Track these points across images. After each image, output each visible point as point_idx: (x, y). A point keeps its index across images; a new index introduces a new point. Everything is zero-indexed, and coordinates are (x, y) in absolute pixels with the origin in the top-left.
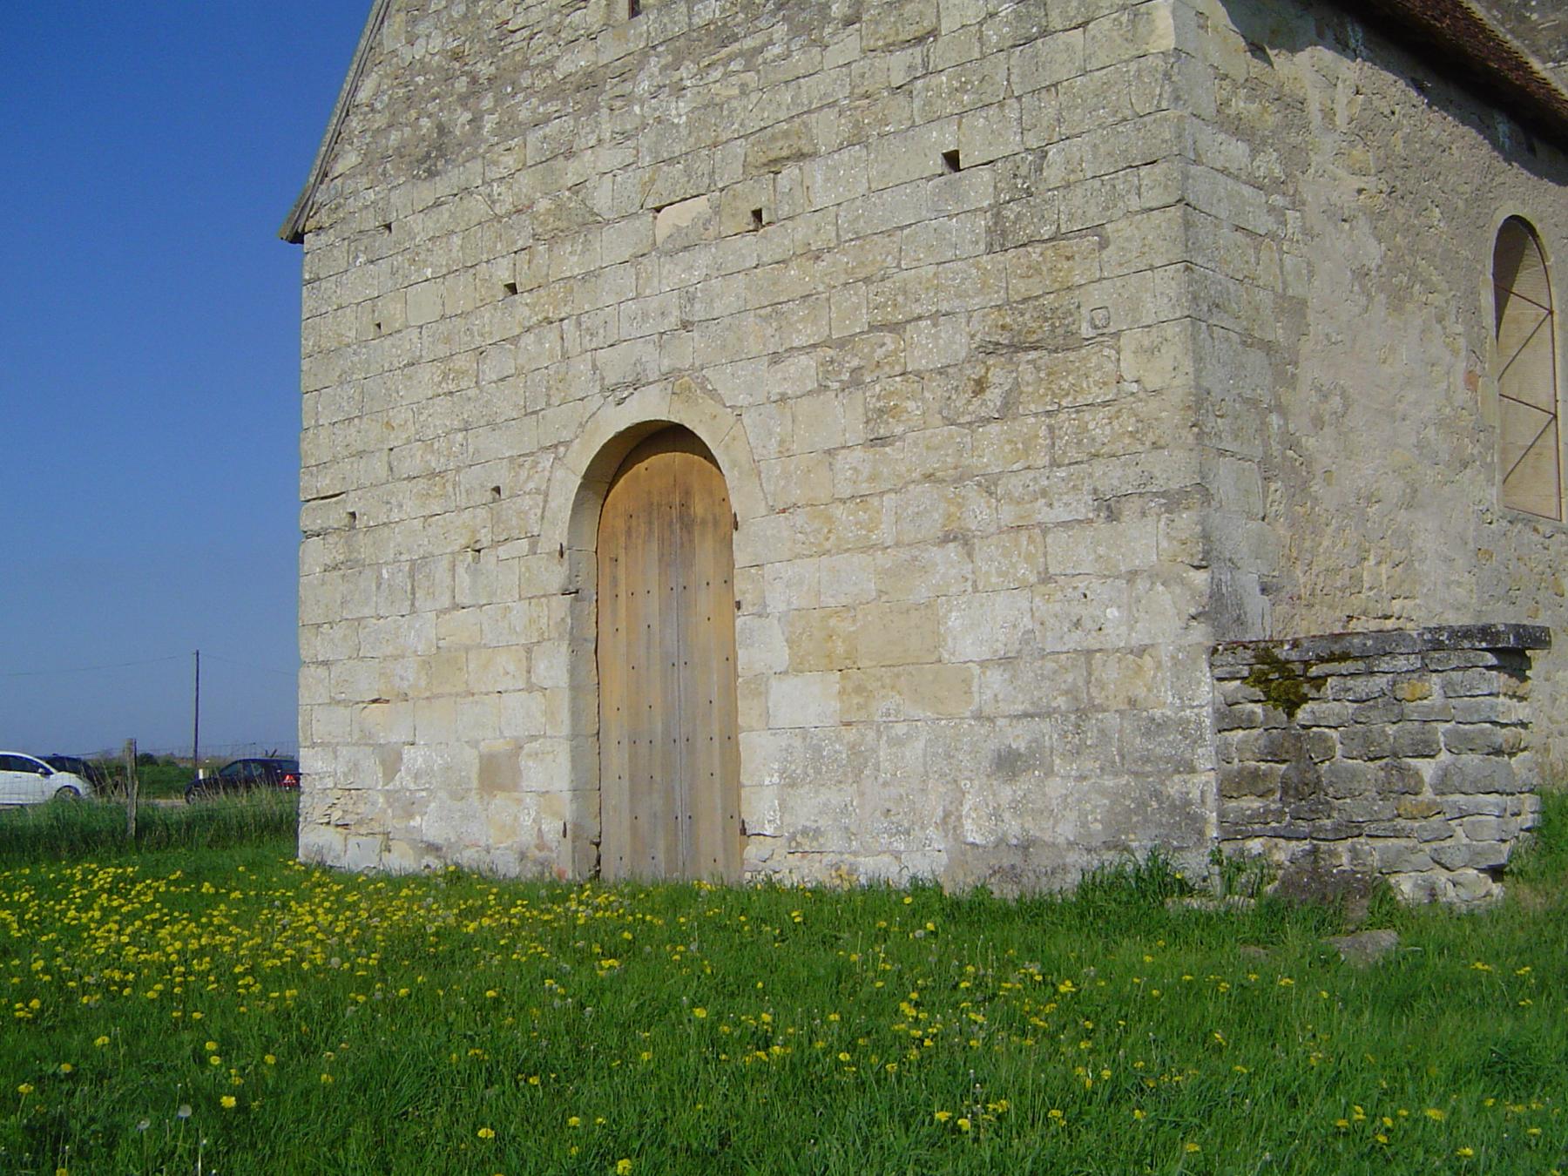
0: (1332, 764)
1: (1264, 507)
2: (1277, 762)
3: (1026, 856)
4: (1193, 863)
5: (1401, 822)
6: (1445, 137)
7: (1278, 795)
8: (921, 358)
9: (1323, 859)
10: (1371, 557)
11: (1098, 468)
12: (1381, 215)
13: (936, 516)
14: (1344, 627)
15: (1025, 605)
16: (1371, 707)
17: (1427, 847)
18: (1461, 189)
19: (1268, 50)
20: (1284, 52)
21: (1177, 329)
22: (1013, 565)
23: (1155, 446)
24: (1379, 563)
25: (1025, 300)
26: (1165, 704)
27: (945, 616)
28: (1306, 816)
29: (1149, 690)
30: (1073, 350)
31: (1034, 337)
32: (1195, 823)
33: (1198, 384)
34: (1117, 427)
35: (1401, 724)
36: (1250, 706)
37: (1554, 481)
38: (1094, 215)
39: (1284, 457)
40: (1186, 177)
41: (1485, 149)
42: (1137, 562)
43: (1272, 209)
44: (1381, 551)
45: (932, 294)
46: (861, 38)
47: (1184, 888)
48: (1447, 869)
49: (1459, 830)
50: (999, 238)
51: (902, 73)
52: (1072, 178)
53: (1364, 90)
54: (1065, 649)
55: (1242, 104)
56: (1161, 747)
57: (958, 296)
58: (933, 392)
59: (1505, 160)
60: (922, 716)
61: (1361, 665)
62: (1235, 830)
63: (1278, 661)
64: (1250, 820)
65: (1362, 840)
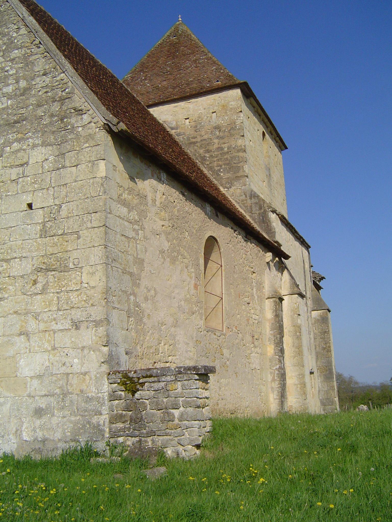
0: (146, 412)
1: (128, 326)
2: (129, 411)
3: (44, 445)
4: (100, 446)
5: (168, 431)
6: (190, 210)
7: (129, 422)
8: (15, 271)
9: (143, 443)
10: (162, 343)
11: (73, 312)
12: (170, 233)
13: (18, 326)
14: (153, 366)
15: (47, 357)
16: (159, 393)
17: (176, 439)
18: (195, 227)
19: (136, 179)
20: (141, 180)
21: (101, 267)
22: (43, 344)
23: (92, 305)
24: (165, 345)
25: (52, 254)
26: (92, 392)
27: (19, 361)
28: (138, 429)
29: (87, 387)
30: (67, 272)
31: (54, 267)
32: (101, 432)
33: (107, 285)
34: (80, 298)
35: (168, 398)
36: (121, 392)
37: (221, 319)
38: (76, 228)
39: (135, 309)
40: (106, 218)
41: (203, 215)
42: (85, 344)
43: (134, 230)
44: (166, 341)
45: (20, 250)
46: (2, 162)
47: (97, 454)
48: (183, 446)
49: (186, 433)
50: (44, 233)
51: (15, 176)
52: (70, 215)
53: (166, 194)
54: (59, 373)
55: (126, 196)
56: (91, 406)
57: (29, 251)
58: (19, 283)
59: (209, 218)
60: (9, 395)
61: (156, 379)
62: (114, 434)
63: (129, 377)
64: (120, 431)
65: (156, 437)
